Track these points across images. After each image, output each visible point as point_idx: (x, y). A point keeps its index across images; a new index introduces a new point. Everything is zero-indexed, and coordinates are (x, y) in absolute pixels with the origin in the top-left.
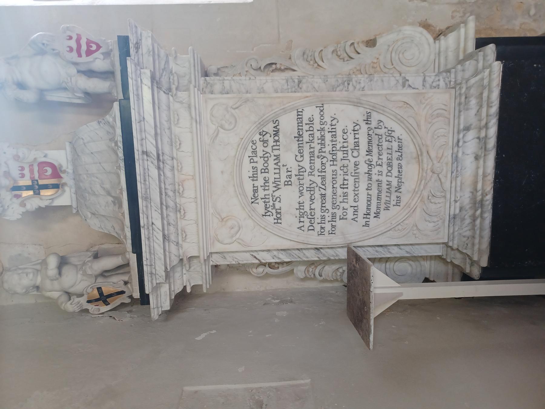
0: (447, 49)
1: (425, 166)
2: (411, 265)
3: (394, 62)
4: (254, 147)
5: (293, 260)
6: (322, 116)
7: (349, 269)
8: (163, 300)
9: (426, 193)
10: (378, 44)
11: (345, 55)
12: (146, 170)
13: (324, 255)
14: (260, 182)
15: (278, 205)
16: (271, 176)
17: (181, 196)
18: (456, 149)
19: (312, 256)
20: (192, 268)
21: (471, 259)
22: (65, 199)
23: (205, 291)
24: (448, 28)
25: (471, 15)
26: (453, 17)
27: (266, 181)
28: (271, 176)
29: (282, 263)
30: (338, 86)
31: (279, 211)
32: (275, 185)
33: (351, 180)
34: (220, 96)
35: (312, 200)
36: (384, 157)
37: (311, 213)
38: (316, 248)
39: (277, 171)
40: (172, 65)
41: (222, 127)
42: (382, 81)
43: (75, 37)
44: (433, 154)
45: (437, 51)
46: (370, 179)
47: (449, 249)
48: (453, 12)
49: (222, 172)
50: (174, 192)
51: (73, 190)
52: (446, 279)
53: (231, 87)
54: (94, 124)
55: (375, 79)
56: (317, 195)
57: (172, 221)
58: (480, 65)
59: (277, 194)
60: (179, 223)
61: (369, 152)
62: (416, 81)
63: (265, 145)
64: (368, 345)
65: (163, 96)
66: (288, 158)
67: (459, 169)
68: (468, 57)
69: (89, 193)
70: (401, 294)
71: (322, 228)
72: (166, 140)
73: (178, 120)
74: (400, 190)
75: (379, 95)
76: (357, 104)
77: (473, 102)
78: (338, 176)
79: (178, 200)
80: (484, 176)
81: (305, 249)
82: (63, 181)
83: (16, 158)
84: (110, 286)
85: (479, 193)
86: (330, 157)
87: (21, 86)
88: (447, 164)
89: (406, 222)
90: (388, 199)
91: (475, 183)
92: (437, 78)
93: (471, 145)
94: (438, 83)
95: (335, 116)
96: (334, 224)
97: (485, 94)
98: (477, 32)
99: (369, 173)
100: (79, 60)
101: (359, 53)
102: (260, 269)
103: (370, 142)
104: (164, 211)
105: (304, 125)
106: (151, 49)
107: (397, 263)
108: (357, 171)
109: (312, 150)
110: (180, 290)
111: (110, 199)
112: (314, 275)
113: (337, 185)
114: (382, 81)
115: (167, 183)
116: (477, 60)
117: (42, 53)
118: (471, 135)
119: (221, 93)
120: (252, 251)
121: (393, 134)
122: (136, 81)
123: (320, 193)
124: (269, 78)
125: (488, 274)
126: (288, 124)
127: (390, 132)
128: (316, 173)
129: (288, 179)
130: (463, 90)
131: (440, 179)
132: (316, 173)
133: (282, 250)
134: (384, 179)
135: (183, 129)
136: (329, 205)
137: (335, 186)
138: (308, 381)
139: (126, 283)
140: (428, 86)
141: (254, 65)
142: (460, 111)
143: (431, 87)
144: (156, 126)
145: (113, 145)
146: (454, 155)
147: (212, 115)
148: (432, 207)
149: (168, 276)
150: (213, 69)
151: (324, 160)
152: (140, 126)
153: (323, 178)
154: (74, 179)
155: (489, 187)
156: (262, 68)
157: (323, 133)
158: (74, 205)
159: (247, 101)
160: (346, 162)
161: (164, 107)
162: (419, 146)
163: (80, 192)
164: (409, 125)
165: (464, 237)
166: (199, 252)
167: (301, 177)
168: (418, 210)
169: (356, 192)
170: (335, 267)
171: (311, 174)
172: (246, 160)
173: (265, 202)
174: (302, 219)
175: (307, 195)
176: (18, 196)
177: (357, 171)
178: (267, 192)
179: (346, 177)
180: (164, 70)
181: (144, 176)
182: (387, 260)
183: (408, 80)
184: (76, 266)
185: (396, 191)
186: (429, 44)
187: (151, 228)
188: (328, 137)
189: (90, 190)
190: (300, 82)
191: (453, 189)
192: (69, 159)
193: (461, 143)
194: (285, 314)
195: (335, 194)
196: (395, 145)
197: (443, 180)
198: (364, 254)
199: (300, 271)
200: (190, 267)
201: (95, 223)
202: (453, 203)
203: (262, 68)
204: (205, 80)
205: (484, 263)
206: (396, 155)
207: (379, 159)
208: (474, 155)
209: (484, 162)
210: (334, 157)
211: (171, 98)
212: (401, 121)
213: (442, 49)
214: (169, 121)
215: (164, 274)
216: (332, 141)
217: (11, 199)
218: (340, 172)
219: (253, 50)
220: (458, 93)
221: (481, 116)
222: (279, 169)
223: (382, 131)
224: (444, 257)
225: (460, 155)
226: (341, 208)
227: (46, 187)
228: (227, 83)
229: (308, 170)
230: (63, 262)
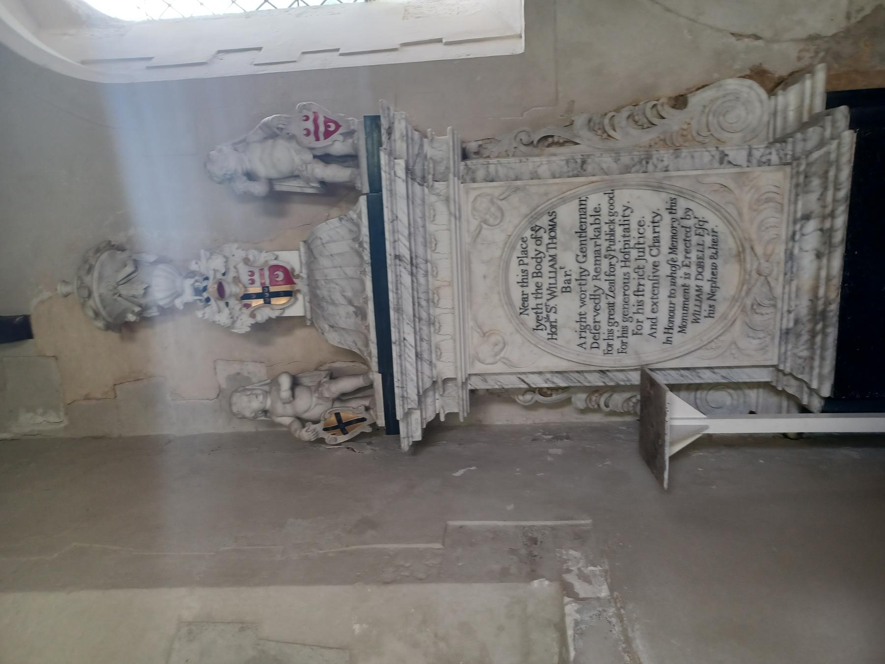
1: (748, 266)
2: (731, 395)
3: (712, 128)
4: (524, 246)
5: (571, 385)
6: (611, 205)
7: (642, 397)
8: (414, 429)
9: (748, 302)
10: (689, 105)
11: (645, 120)
12: (398, 276)
13: (611, 380)
14: (531, 289)
15: (552, 317)
16: (545, 282)
17: (436, 305)
18: (790, 244)
19: (596, 380)
20: (447, 392)
21: (809, 388)
22: (297, 309)
23: (462, 420)
24: (792, 74)
25: (820, 62)
26: (799, 59)
27: (539, 287)
28: (545, 282)
29: (557, 389)
30: (634, 166)
31: (554, 324)
32: (549, 292)
33: (648, 285)
34: (484, 184)
35: (596, 310)
36: (694, 255)
37: (595, 326)
38: (602, 371)
39: (553, 275)
40: (428, 150)
41: (485, 222)
42: (693, 157)
43: (312, 118)
44: (759, 250)
46: (674, 284)
47: (781, 375)
49: (485, 277)
50: (428, 301)
51: (307, 298)
52: (778, 412)
54: (335, 222)
55: (683, 154)
56: (603, 304)
57: (425, 337)
58: (828, 133)
59: (552, 303)
60: (433, 338)
61: (673, 249)
62: (738, 155)
63: (539, 242)
64: (660, 479)
65: (417, 188)
66: (568, 259)
67: (795, 270)
68: (815, 120)
69: (327, 302)
70: (707, 427)
71: (609, 345)
72: (420, 240)
73: (434, 216)
74: (714, 298)
75: (687, 176)
76: (658, 188)
77: (816, 182)
78: (631, 280)
79: (431, 311)
80: (828, 279)
81: (586, 372)
82: (297, 287)
83: (246, 261)
84: (351, 410)
85: (821, 302)
86: (620, 256)
87: (250, 176)
88: (778, 263)
89: (721, 338)
90: (697, 309)
91: (815, 289)
92: (768, 151)
93: (811, 239)
94: (768, 157)
95: (628, 205)
96: (625, 340)
97: (832, 173)
98: (829, 80)
99: (672, 277)
100: (318, 145)
101: (663, 118)
102: (528, 397)
103: (674, 237)
104: (417, 324)
105: (588, 217)
106: (405, 133)
107: (711, 392)
108: (656, 274)
109: (598, 248)
110: (432, 418)
111: (351, 309)
112: (599, 405)
114: (693, 157)
117: (273, 136)
118: (812, 225)
119: (486, 180)
120: (520, 373)
122: (390, 174)
123: (607, 301)
124: (544, 159)
125: (831, 406)
126: (568, 215)
127: (701, 223)
128: (603, 277)
129: (566, 285)
130: (802, 168)
131: (768, 283)
132: (603, 277)
133: (557, 372)
134: (692, 283)
135: (440, 225)
136: (618, 317)
137: (627, 293)
138: (589, 521)
139: (367, 409)
140: (754, 161)
141: (525, 139)
142: (797, 195)
143: (760, 164)
144: (409, 224)
145: (357, 246)
146: (788, 252)
147: (474, 209)
148: (758, 319)
149: (420, 402)
150: (473, 146)
152: (393, 227)
153: (612, 283)
154: (308, 285)
155: (834, 294)
156: (535, 142)
157: (612, 227)
158: (309, 316)
159: (517, 189)
160: (641, 263)
161: (418, 201)
162: (740, 240)
163: (315, 300)
164: (727, 215)
165: (800, 358)
166: (456, 374)
167: (583, 282)
168: (738, 324)
169: (655, 301)
170: (627, 395)
171: (596, 278)
172: (514, 262)
173: (536, 313)
174: (583, 335)
175: (590, 305)
176: (247, 306)
177: (656, 274)
178: (539, 301)
179: (642, 282)
180: (418, 155)
181: (397, 284)
182: (698, 387)
183: (727, 155)
184: (309, 387)
185: (708, 299)
186: (761, 101)
187: (402, 344)
188: (619, 231)
189: (328, 299)
190: (584, 162)
191: (786, 296)
192: (304, 261)
193: (797, 237)
194: (559, 451)
195: (626, 303)
196: (708, 240)
197: (772, 284)
198: (661, 379)
199: (580, 400)
200: (444, 391)
201: (334, 338)
202: (785, 314)
203: (535, 142)
204: (466, 165)
205: (826, 391)
206: (708, 252)
207: (686, 257)
208: (815, 252)
209: (829, 260)
210: (627, 257)
211: (426, 190)
212: (716, 209)
214: (423, 217)
215: (416, 398)
216: (624, 236)
217: (240, 309)
219: (522, 115)
220: (794, 171)
221: (824, 201)
222: (555, 272)
223: (690, 223)
224: (774, 384)
226: (635, 321)
227: (278, 294)
228: (492, 168)
229: (593, 273)
230: (295, 383)
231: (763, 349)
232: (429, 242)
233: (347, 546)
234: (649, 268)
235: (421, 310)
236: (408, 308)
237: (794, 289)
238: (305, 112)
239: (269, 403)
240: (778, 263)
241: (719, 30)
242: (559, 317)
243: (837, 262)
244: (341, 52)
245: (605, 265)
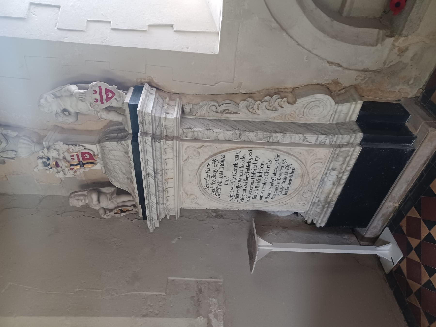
0: (341, 112)
4: (209, 166)
6: (250, 155)
14: (211, 181)
15: (219, 191)
18: (324, 176)
26: (356, 80)
27: (214, 181)
28: (217, 180)
33: (261, 185)
44: (311, 176)
45: (335, 110)
48: (357, 76)
53: (198, 135)
55: (287, 137)
56: (241, 189)
61: (274, 174)
66: (228, 174)
67: (323, 185)
77: (341, 159)
80: (334, 193)
86: (251, 175)
91: (329, 194)
92: (325, 139)
99: (272, 183)
103: (276, 170)
106: (151, 121)
109: (242, 171)
113: (254, 187)
114: (291, 138)
115: (159, 181)
116: (351, 137)
121: (290, 166)
124: (222, 132)
126: (230, 157)
128: (242, 181)
130: (337, 152)
138: (222, 280)
142: (332, 161)
151: (248, 176)
153: (246, 184)
155: (335, 199)
160: (260, 178)
175: (236, 190)
176: (72, 169)
179: (259, 184)
186: (331, 105)
188: (252, 166)
191: (317, 192)
193: (327, 175)
196: (290, 171)
202: (315, 198)
213: (338, 111)
218: (256, 181)
220: (333, 152)
221: (342, 167)
225: (325, 179)
229: (238, 179)
231: (304, 205)
232: (164, 162)
233: (128, 292)
234: (263, 180)
235: (159, 188)
236: (153, 190)
237: (321, 191)
238: (94, 88)
239: (87, 202)
240: (318, 180)
241: (322, 59)
242: (222, 192)
243: (339, 190)
244: (112, 26)
245: (244, 177)
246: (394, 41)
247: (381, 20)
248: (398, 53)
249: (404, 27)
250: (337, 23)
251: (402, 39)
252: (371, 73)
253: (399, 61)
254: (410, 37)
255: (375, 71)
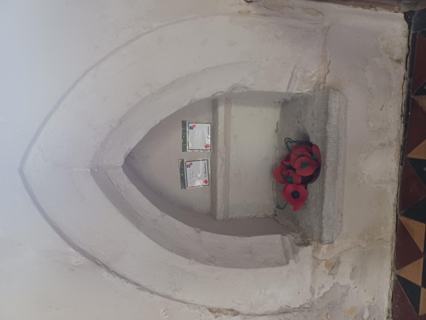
246: (314, 251)
247: (276, 218)
248: (327, 271)
249: (321, 227)
250: (209, 234)
251: (324, 248)
252: (295, 314)
253: (334, 284)
254: (336, 242)
255: (301, 309)
